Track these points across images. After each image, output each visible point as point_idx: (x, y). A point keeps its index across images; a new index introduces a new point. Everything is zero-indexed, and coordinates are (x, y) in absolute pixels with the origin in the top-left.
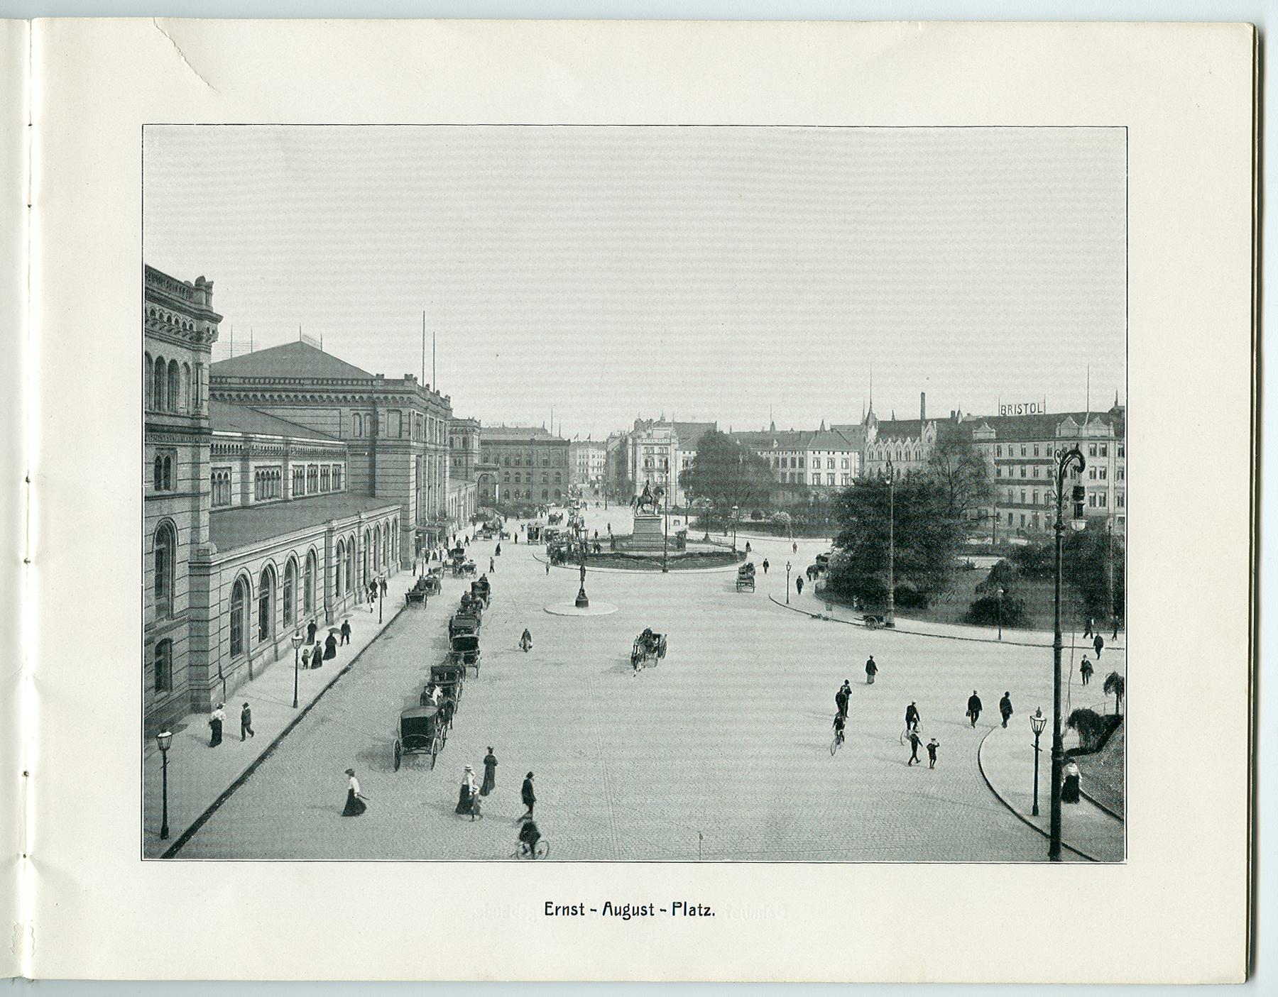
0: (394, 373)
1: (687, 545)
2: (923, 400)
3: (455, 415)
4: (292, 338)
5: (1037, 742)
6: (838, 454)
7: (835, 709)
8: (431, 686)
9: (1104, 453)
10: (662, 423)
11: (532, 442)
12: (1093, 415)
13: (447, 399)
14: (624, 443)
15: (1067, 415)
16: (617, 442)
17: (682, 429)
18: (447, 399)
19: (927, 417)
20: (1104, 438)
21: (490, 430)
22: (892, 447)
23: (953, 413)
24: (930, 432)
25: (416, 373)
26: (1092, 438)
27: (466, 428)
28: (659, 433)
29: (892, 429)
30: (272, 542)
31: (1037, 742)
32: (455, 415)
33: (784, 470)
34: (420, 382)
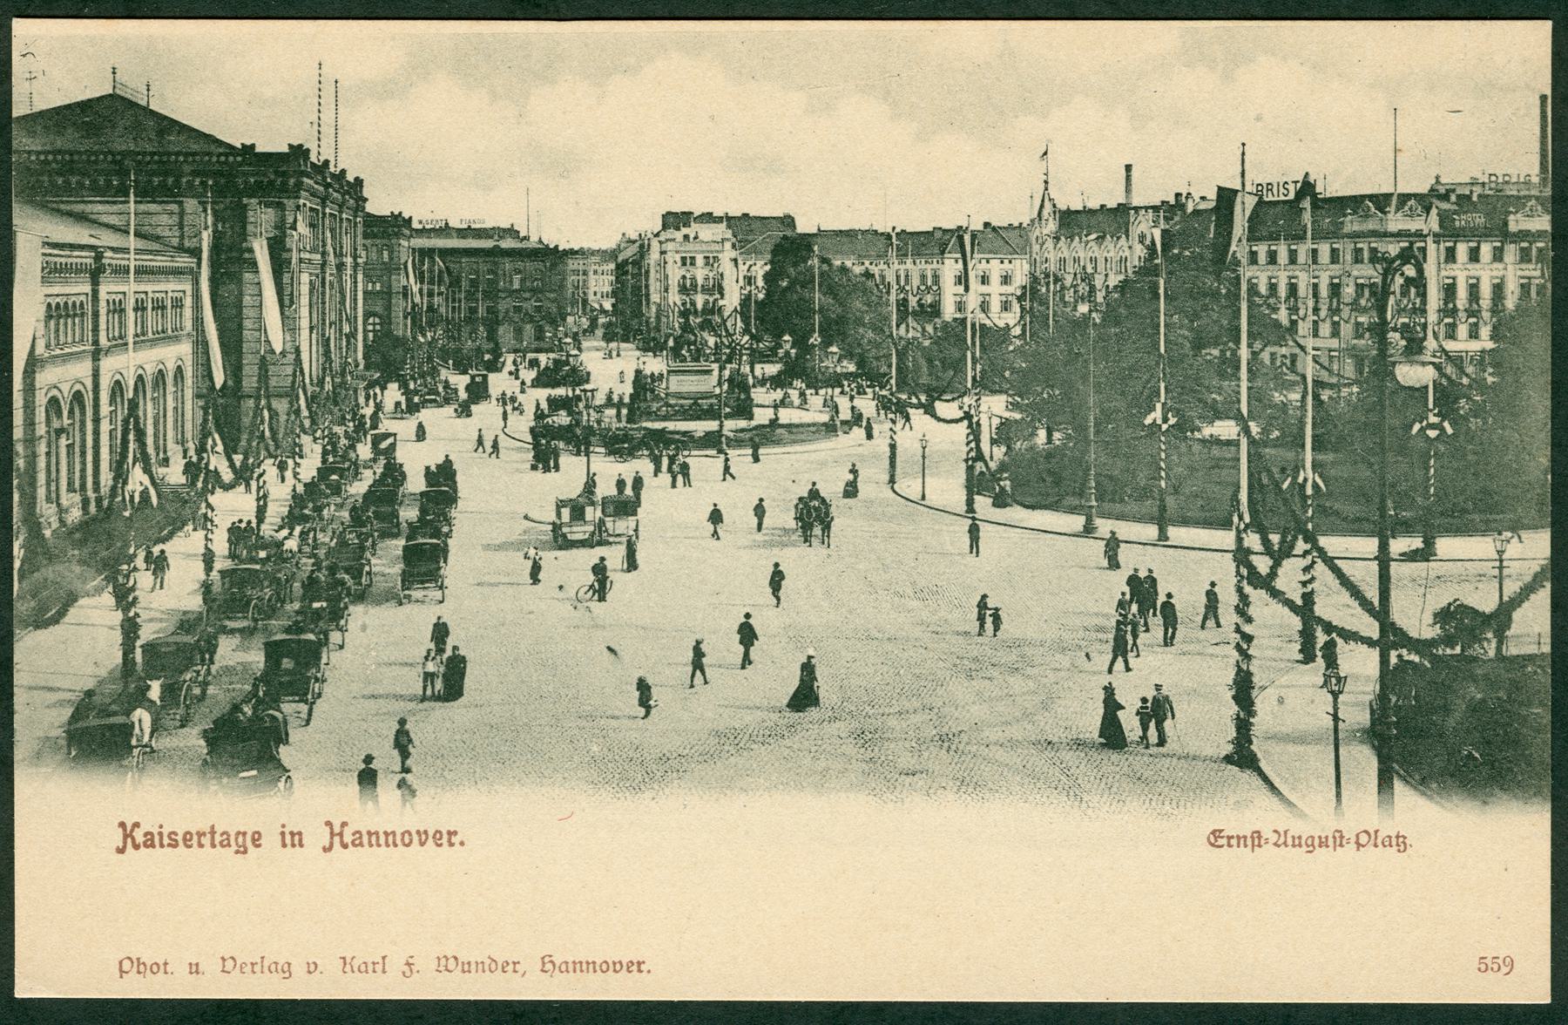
0: (272, 143)
1: (756, 410)
2: (1128, 178)
3: (370, 208)
4: (97, 88)
5: (1336, 708)
6: (995, 263)
7: (756, 520)
8: (391, 259)
10: (708, 218)
11: (496, 252)
12: (1404, 198)
13: (359, 182)
14: (644, 250)
15: (1363, 197)
16: (634, 248)
17: (743, 227)
18: (359, 182)
19: (1136, 201)
21: (423, 232)
22: (1083, 250)
23: (1178, 195)
24: (1148, 228)
25: (312, 145)
27: (392, 227)
28: (707, 232)
29: (1072, 222)
30: (18, 433)
31: (1336, 708)
32: (370, 208)
33: (1475, 270)
34: (313, 158)
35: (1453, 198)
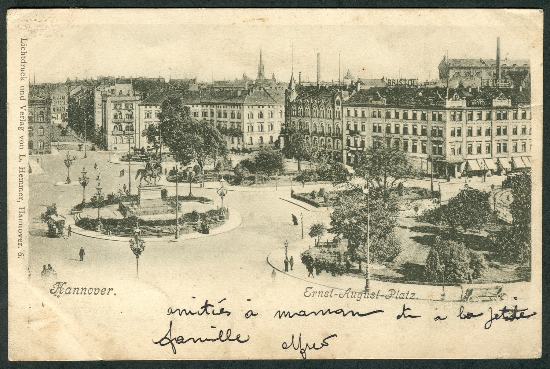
9: (505, 117)
20: (507, 108)
26: (498, 108)
35: (470, 91)
